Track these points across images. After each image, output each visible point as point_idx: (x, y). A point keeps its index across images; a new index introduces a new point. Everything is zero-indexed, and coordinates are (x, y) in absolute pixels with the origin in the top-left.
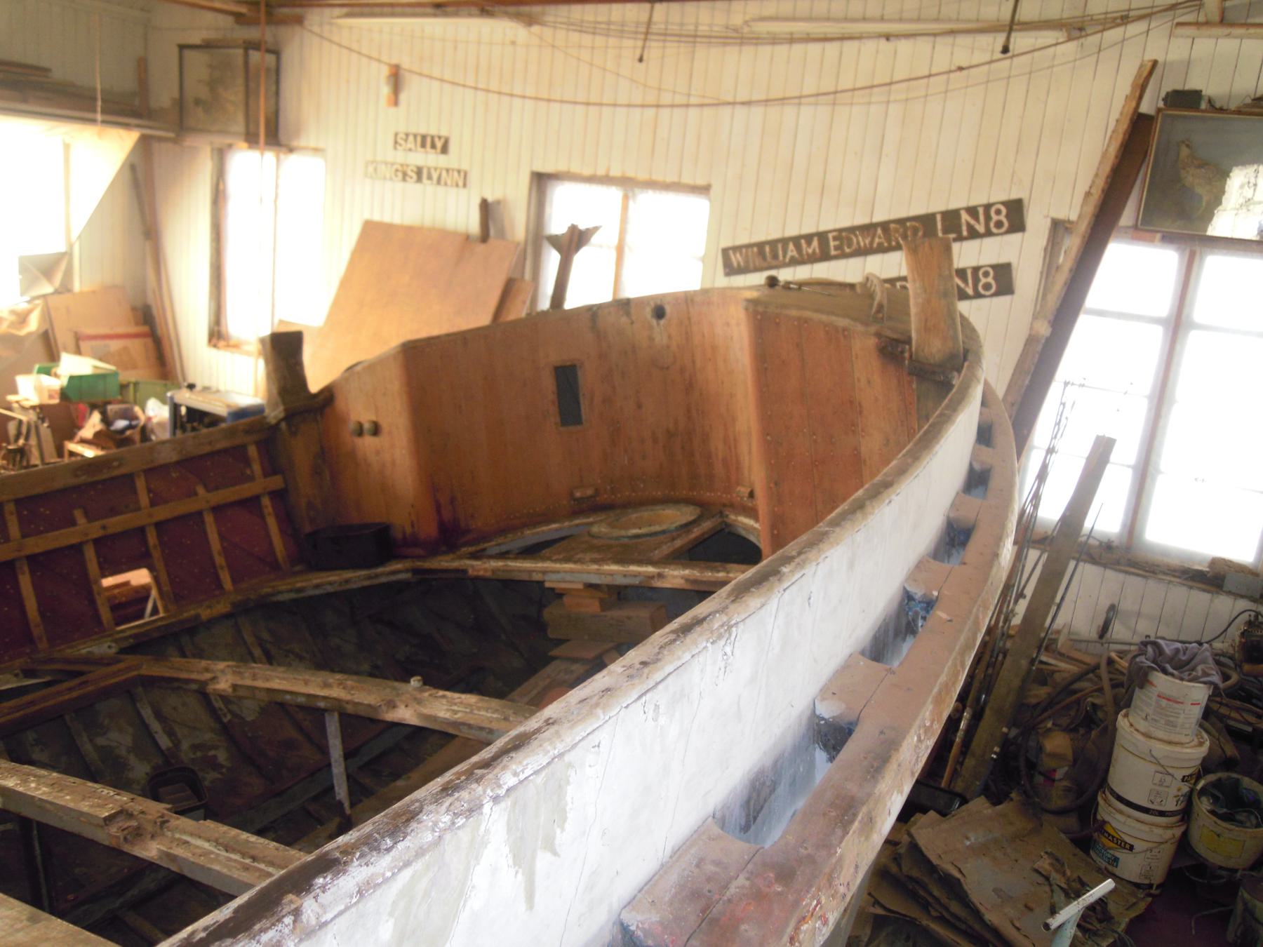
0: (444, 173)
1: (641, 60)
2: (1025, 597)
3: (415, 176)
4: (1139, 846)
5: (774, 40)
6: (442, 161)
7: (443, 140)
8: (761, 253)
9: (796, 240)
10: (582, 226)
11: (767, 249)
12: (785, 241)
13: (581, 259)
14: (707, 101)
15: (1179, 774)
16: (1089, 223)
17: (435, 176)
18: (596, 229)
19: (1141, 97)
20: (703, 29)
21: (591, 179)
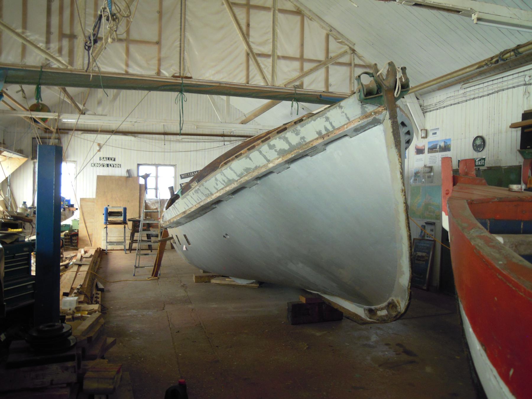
0: (115, 165)
1: (165, 145)
5: (185, 142)
6: (113, 162)
7: (114, 159)
8: (187, 175)
9: (193, 172)
10: (148, 173)
11: (188, 174)
12: (191, 173)
13: (148, 179)
14: (174, 151)
17: (112, 166)
18: (151, 174)
20: (172, 139)
21: (149, 165)
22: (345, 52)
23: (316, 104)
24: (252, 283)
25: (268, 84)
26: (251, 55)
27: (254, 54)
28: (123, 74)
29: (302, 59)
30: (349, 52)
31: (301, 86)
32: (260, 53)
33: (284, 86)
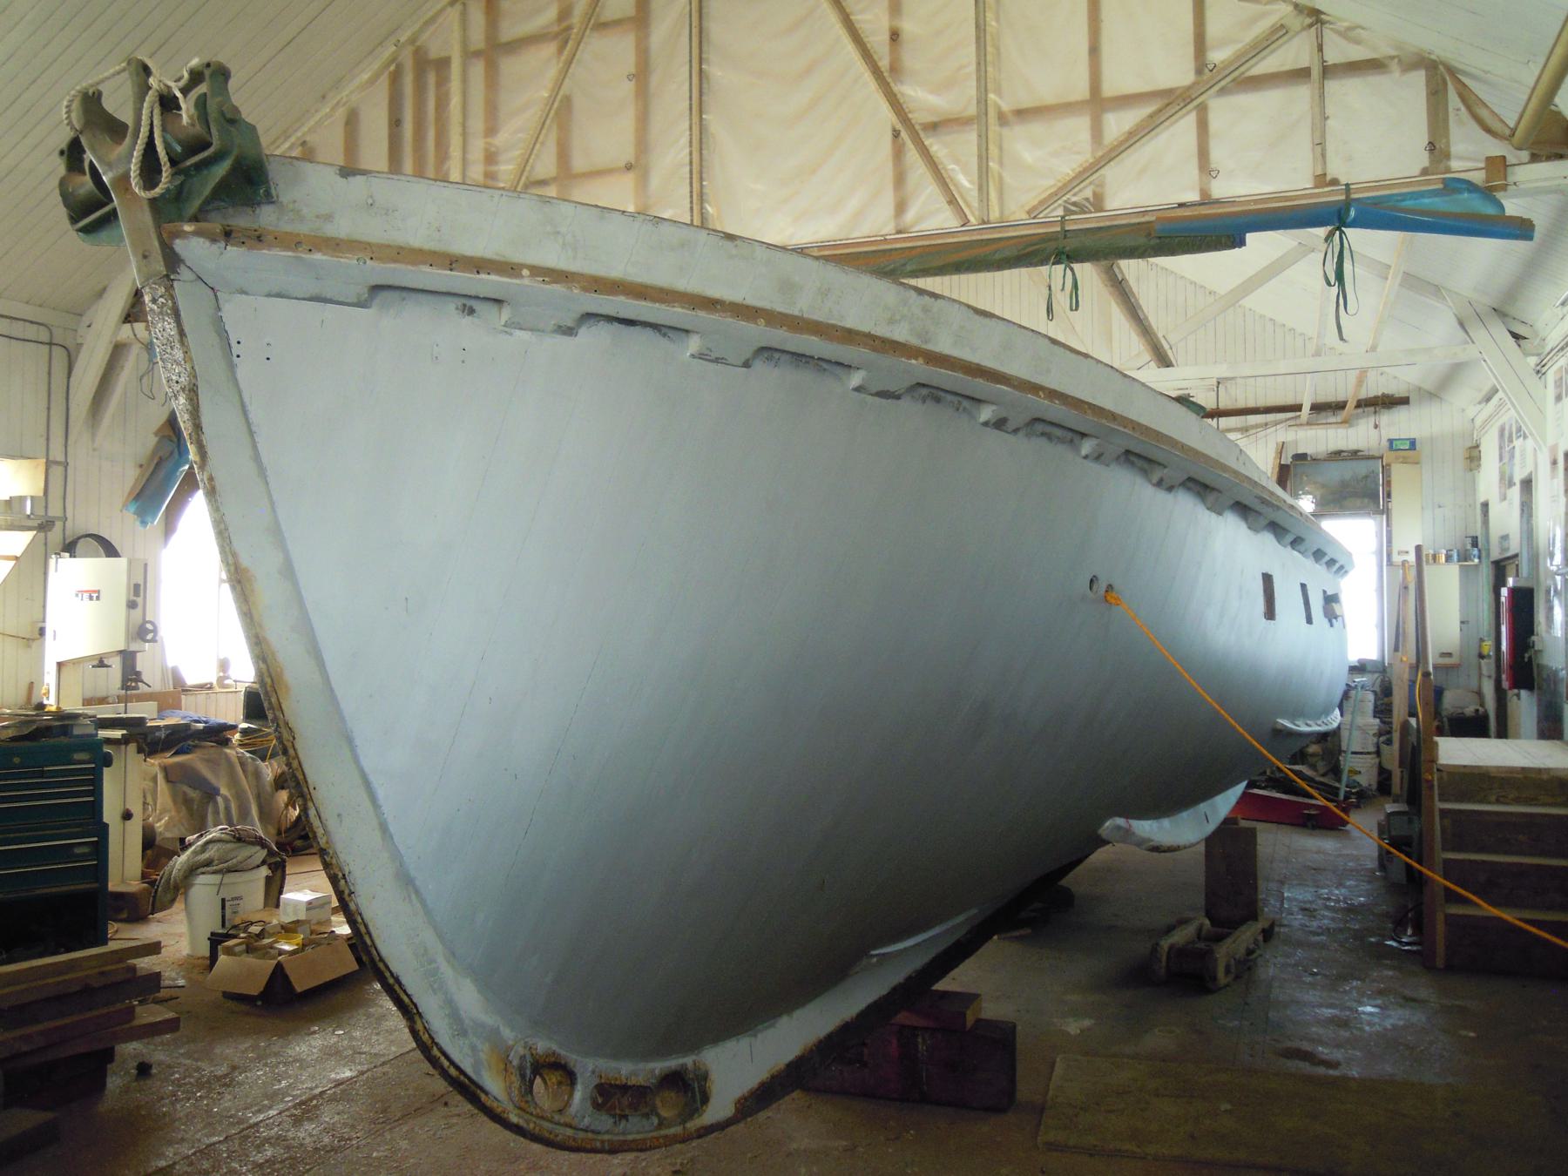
2: (1515, 484)
3: (1164, 483)
4: (1363, 770)
15: (1371, 733)
16: (1117, 303)
19: (1280, 458)
22: (1279, 33)
23: (1203, 252)
24: (173, 867)
25: (969, 221)
26: (904, 135)
27: (917, 127)
28: (1193, 205)
29: (1097, 103)
30: (1296, 22)
31: (1098, 202)
32: (935, 119)
33: (1025, 216)
